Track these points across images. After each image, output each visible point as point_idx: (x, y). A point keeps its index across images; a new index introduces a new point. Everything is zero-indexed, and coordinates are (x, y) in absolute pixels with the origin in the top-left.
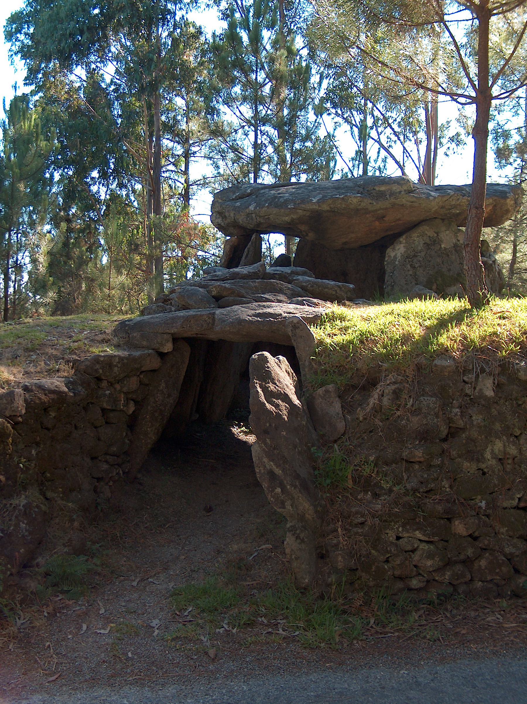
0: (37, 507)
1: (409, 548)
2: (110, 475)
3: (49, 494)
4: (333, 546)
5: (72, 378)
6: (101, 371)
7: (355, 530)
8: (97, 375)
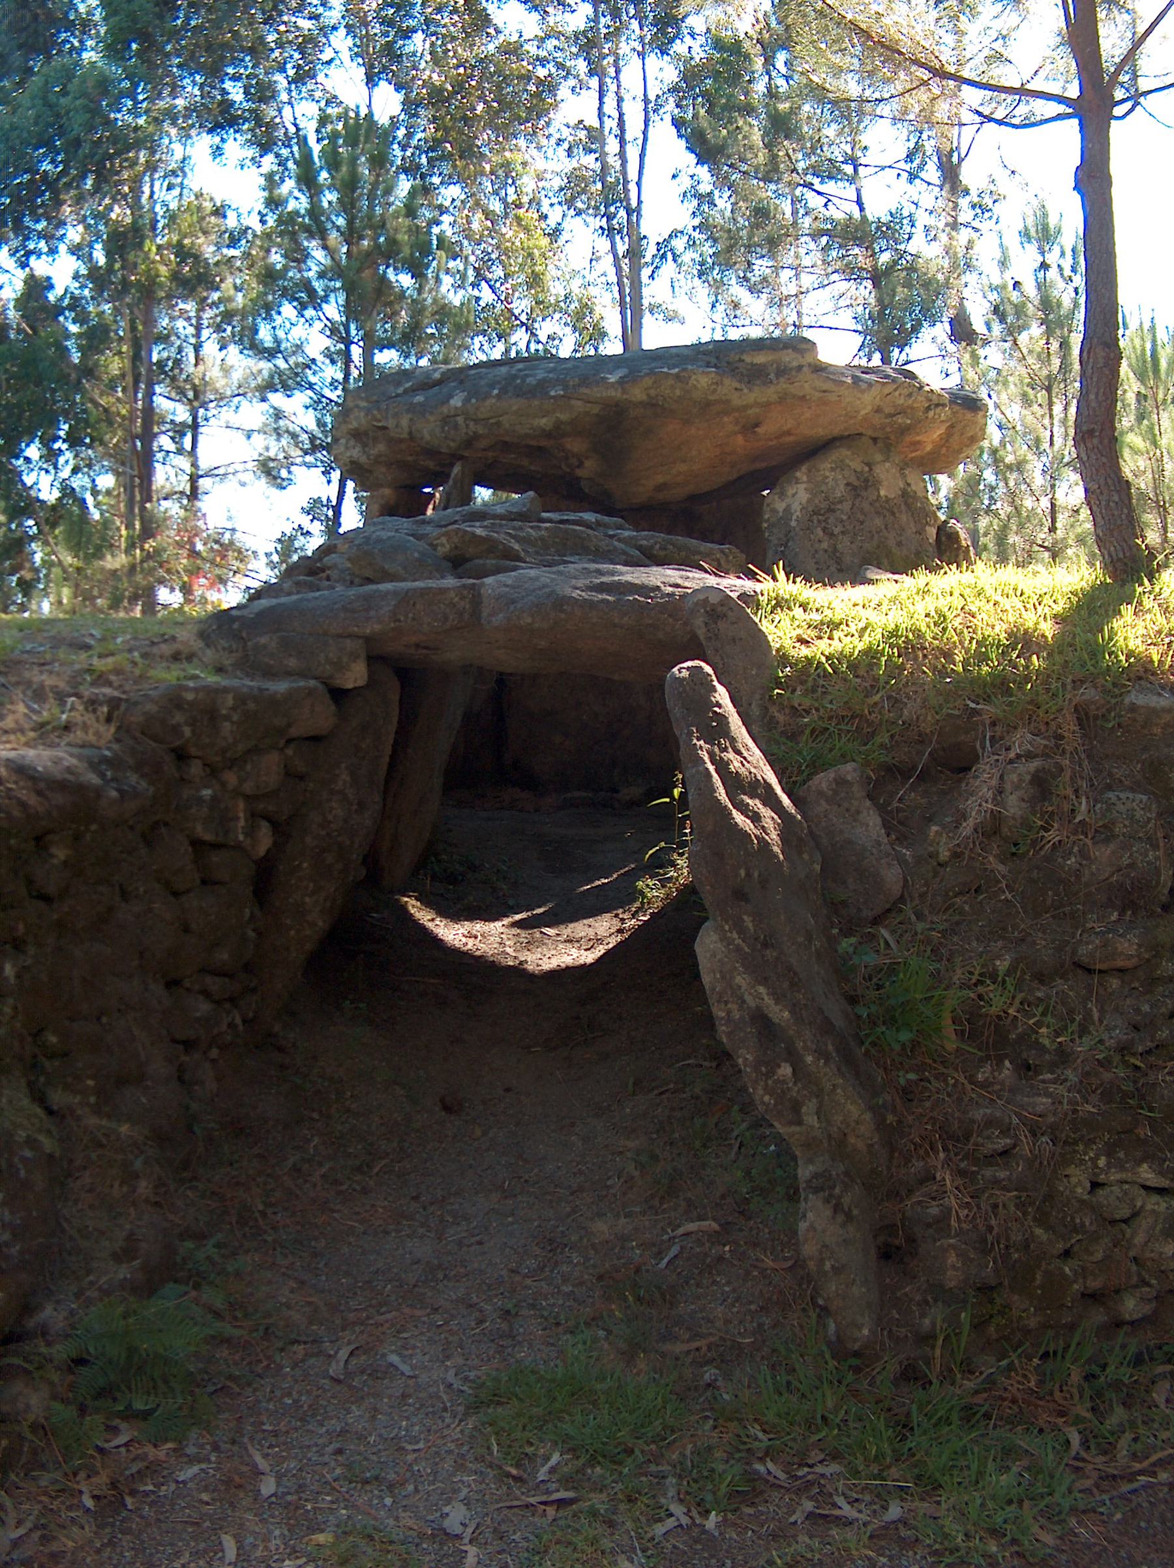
0: (31, 1142)
1: (1125, 1213)
2: (215, 1031)
3: (58, 1098)
4: (929, 1225)
5: (108, 749)
6: (187, 731)
7: (988, 1172)
8: (178, 743)
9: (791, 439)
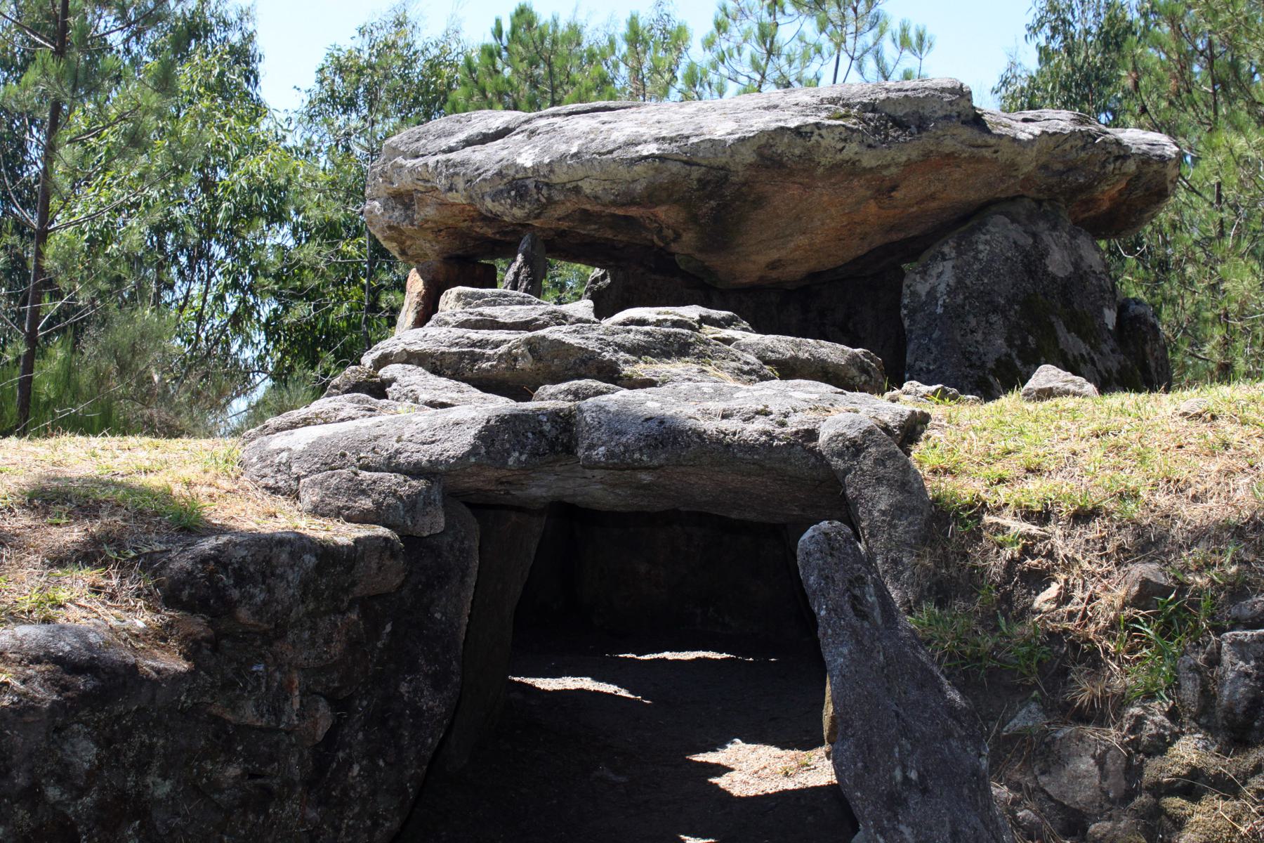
9: (934, 205)
